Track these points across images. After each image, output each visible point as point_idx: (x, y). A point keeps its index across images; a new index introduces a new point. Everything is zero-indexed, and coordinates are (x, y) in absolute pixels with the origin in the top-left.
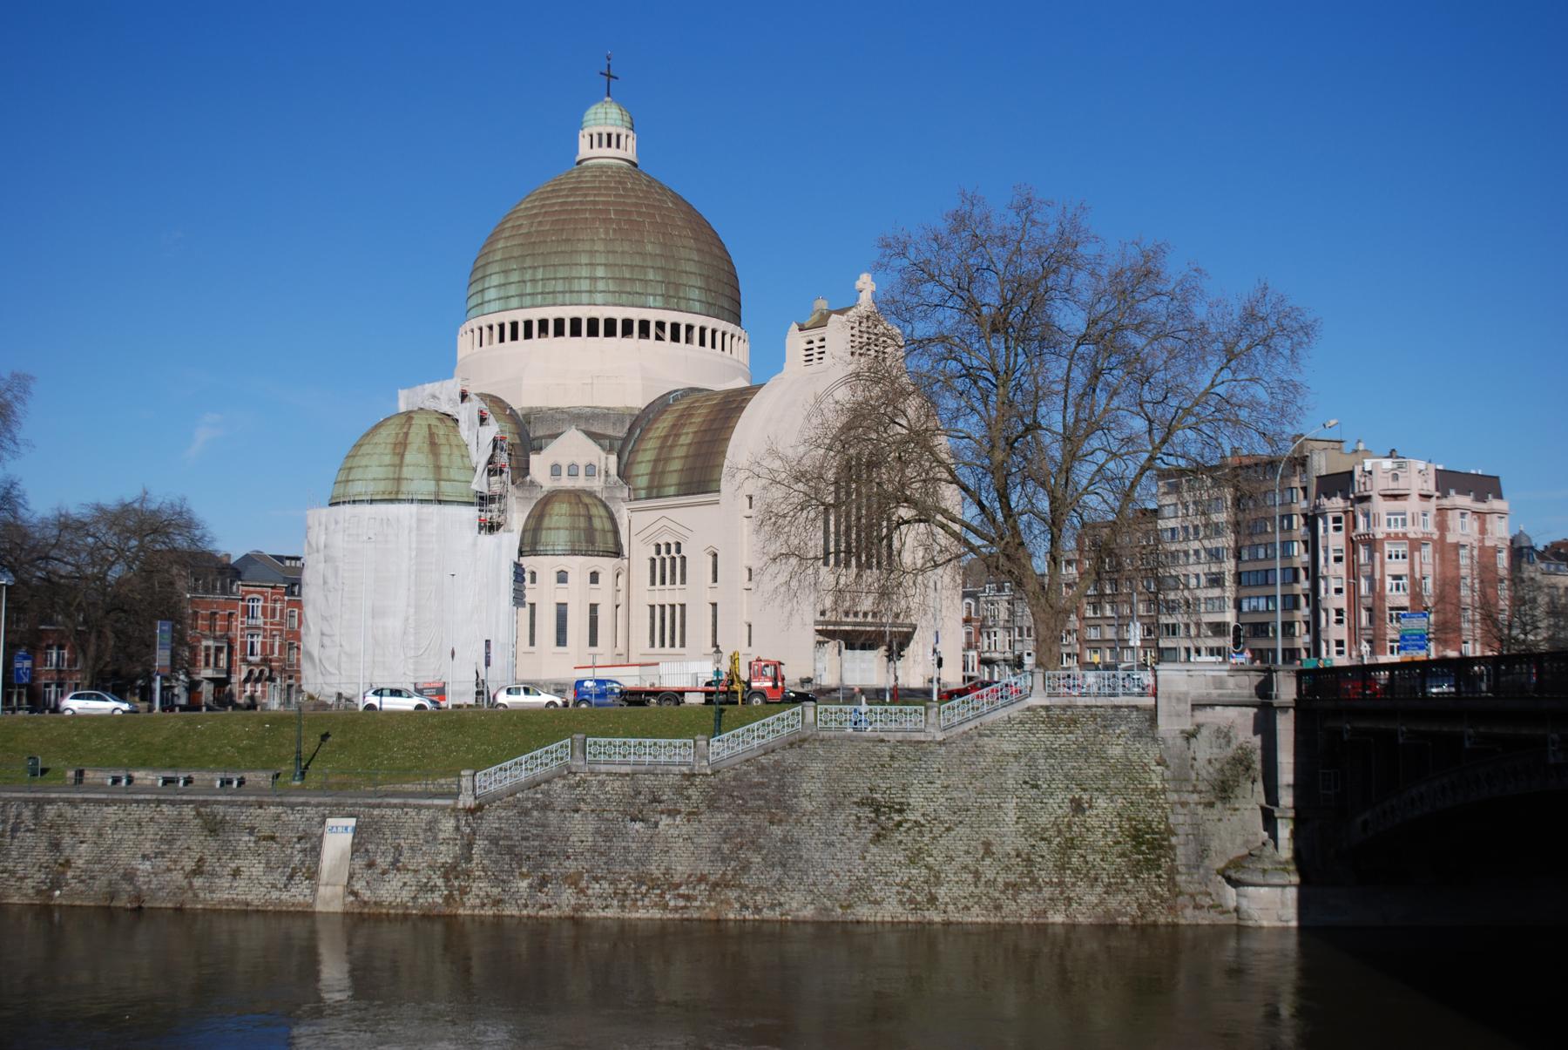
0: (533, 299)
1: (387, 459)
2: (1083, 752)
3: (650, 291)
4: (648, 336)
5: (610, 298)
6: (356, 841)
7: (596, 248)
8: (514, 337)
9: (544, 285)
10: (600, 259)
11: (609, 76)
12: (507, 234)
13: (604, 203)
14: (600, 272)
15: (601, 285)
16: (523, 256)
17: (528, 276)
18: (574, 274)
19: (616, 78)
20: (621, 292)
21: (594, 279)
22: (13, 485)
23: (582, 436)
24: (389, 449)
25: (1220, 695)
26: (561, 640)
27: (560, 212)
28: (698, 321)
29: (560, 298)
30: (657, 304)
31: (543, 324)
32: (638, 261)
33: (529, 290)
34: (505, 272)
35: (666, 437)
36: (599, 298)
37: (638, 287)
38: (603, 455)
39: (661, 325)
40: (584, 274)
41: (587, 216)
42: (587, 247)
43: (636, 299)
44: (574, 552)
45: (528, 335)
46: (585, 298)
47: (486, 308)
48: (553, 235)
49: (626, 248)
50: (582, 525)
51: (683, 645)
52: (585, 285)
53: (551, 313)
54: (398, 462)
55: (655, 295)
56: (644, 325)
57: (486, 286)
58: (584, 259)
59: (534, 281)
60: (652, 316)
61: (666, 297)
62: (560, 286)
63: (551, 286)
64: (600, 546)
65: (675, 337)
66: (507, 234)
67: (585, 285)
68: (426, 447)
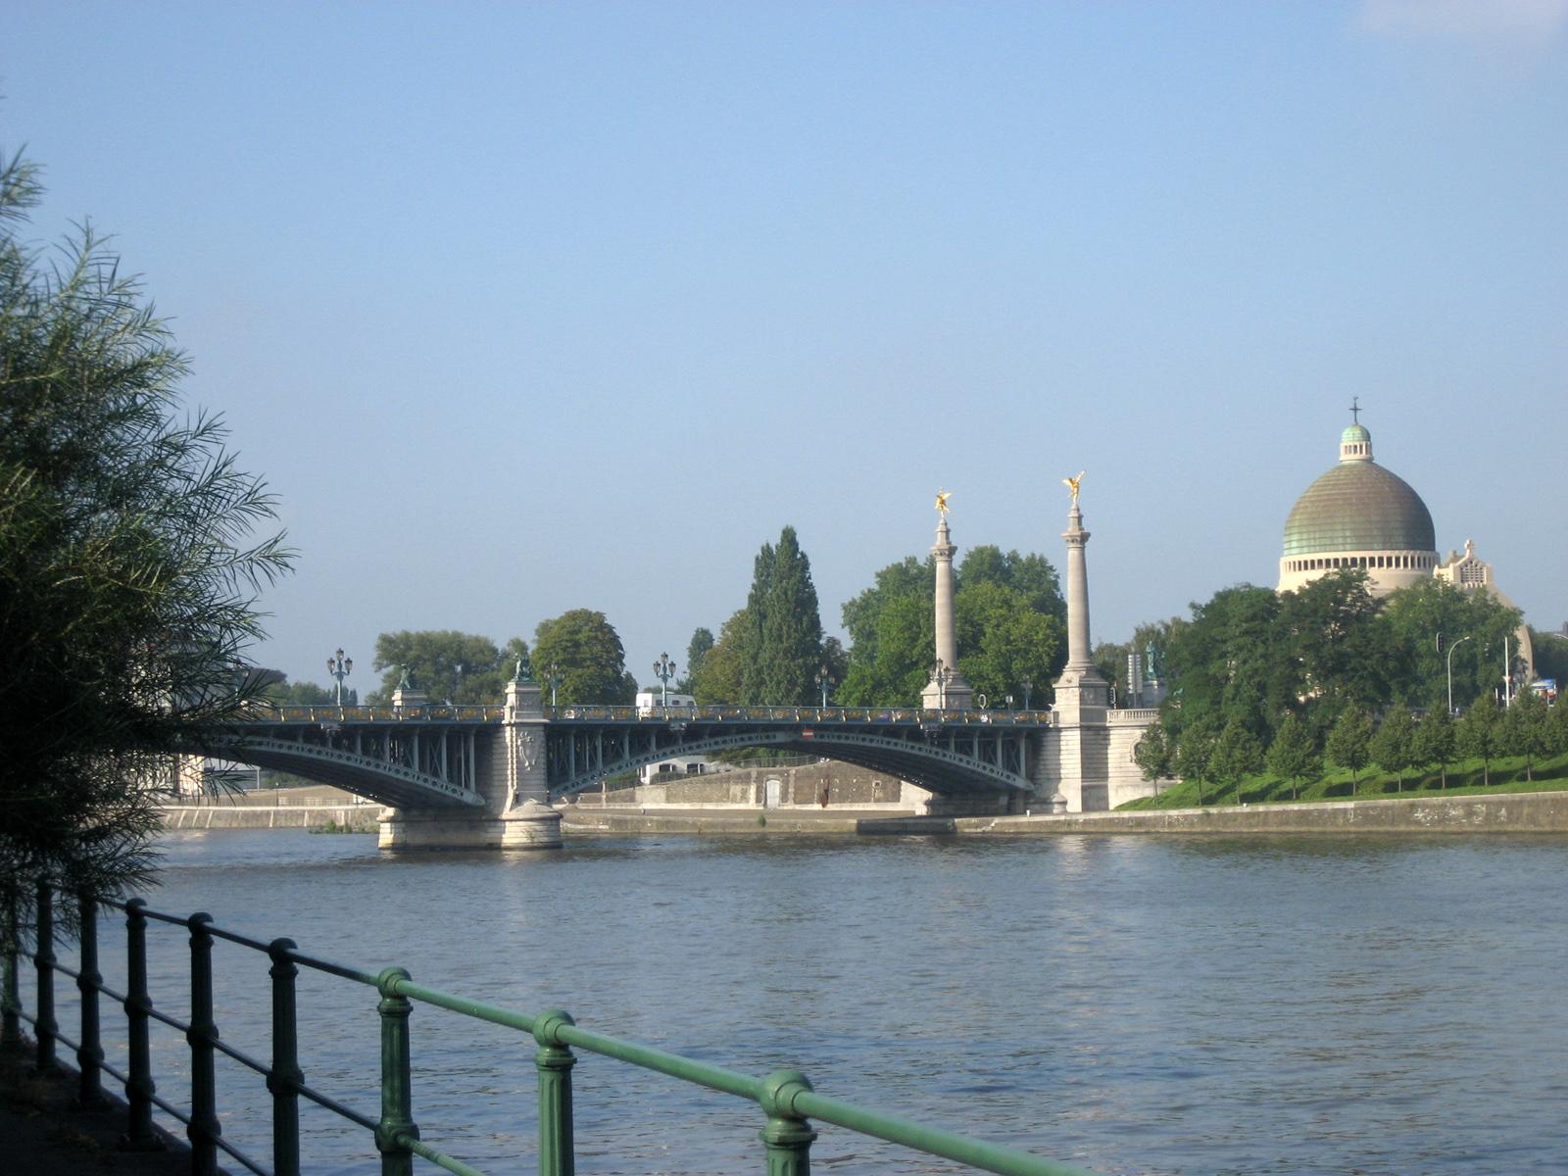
0: (1324, 548)
2: (134, 328)
6: (922, 641)
8: (1300, 569)
12: (1301, 511)
14: (1348, 534)
15: (1349, 540)
16: (1309, 525)
17: (1312, 536)
18: (1335, 535)
19: (194, 374)
20: (1310, 539)
21: (1345, 537)
22: (376, 671)
27: (1328, 500)
31: (1320, 562)
33: (1313, 544)
34: (1300, 533)
36: (1348, 547)
46: (1341, 547)
52: (1340, 540)
56: (1381, 559)
58: (1339, 527)
59: (1314, 539)
63: (1324, 541)
65: (1381, 565)
66: (1301, 511)
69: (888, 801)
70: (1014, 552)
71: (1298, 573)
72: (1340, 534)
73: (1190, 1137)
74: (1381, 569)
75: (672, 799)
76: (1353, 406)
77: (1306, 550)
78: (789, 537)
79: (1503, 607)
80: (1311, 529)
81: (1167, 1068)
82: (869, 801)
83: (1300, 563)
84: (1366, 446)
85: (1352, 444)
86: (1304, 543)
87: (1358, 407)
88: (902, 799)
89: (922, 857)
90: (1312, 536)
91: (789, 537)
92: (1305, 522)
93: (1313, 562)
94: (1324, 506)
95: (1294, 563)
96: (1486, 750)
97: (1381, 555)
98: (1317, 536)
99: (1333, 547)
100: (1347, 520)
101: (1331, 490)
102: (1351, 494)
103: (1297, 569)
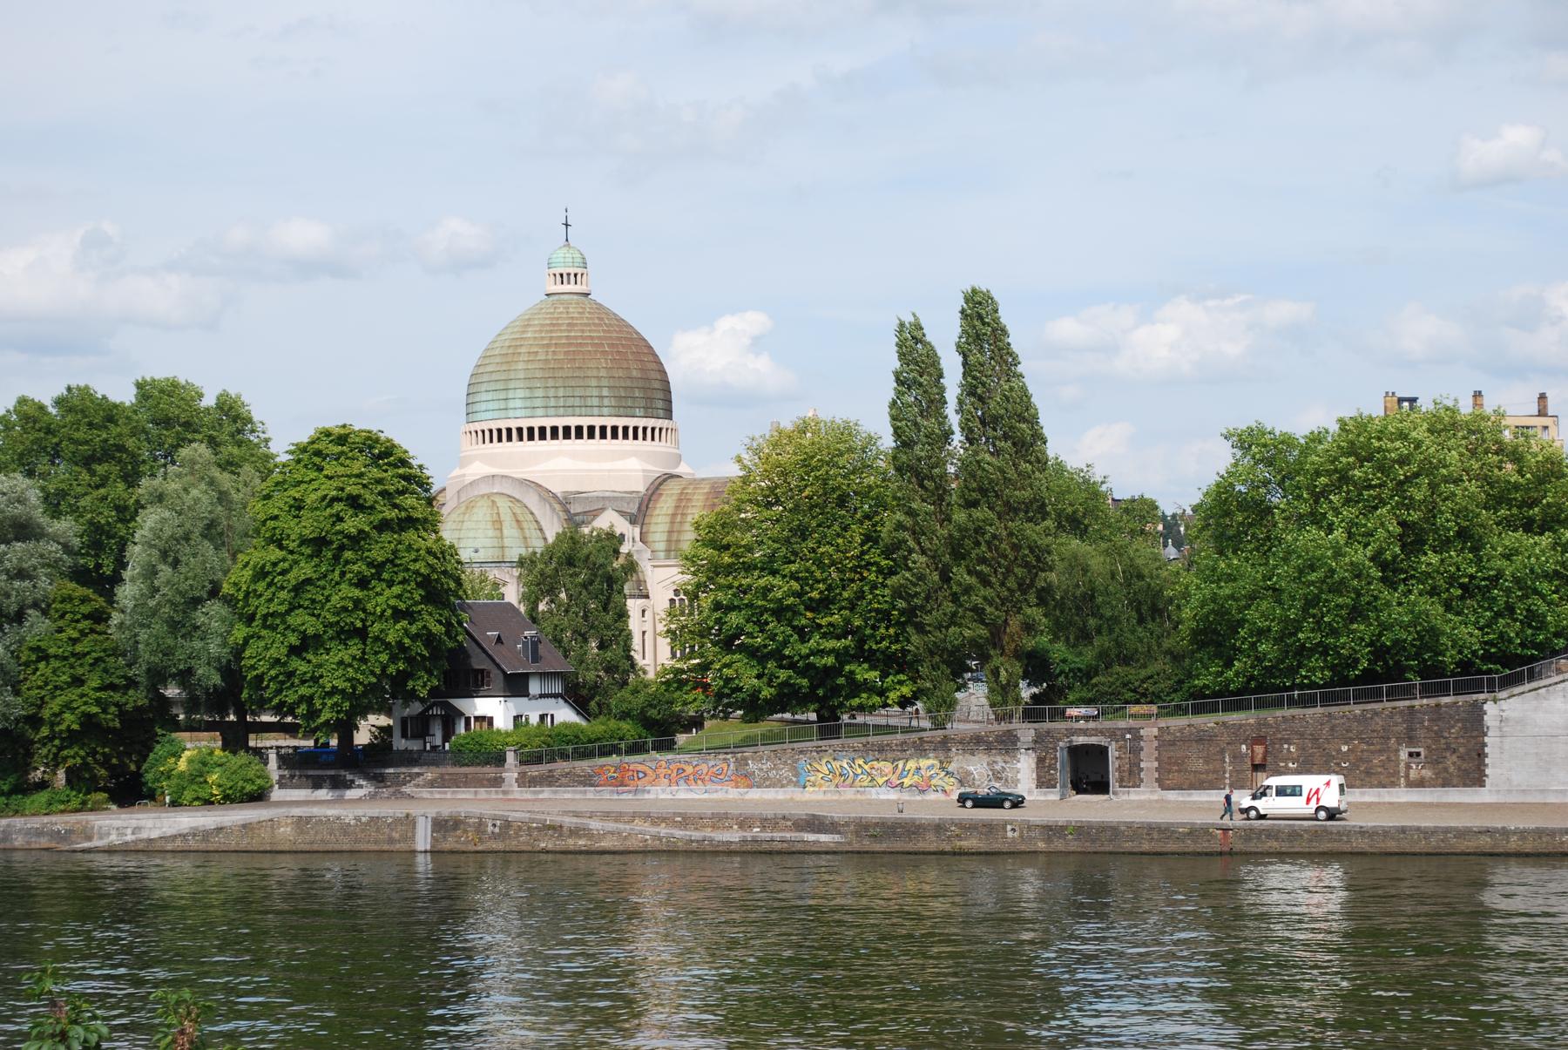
0: (570, 410)
1: (491, 533)
4: (545, 439)
5: (613, 411)
7: (601, 375)
8: (521, 439)
9: (565, 401)
10: (605, 383)
13: (599, 338)
14: (605, 392)
15: (606, 402)
20: (619, 407)
21: (601, 397)
24: (489, 526)
25: (744, 841)
28: (641, 423)
29: (577, 411)
30: (642, 414)
32: (629, 383)
35: (674, 515)
36: (605, 411)
38: (630, 527)
39: (520, 430)
40: (594, 394)
41: (590, 349)
42: (595, 373)
43: (629, 411)
45: (510, 439)
46: (596, 411)
47: (511, 413)
48: (568, 363)
49: (621, 375)
52: (595, 402)
54: (499, 535)
57: (510, 396)
58: (594, 383)
62: (577, 402)
63: (570, 402)
68: (514, 523)
69: (1446, 784)
70: (22, 401)
72: (595, 392)
73: (116, 869)
75: (1175, 777)
79: (1371, 418)
80: (551, 383)
82: (1393, 785)
83: (509, 430)
88: (1488, 781)
89: (201, 829)
90: (551, 393)
92: (539, 374)
96: (278, 709)
98: (561, 393)
99: (586, 409)
100: (603, 373)
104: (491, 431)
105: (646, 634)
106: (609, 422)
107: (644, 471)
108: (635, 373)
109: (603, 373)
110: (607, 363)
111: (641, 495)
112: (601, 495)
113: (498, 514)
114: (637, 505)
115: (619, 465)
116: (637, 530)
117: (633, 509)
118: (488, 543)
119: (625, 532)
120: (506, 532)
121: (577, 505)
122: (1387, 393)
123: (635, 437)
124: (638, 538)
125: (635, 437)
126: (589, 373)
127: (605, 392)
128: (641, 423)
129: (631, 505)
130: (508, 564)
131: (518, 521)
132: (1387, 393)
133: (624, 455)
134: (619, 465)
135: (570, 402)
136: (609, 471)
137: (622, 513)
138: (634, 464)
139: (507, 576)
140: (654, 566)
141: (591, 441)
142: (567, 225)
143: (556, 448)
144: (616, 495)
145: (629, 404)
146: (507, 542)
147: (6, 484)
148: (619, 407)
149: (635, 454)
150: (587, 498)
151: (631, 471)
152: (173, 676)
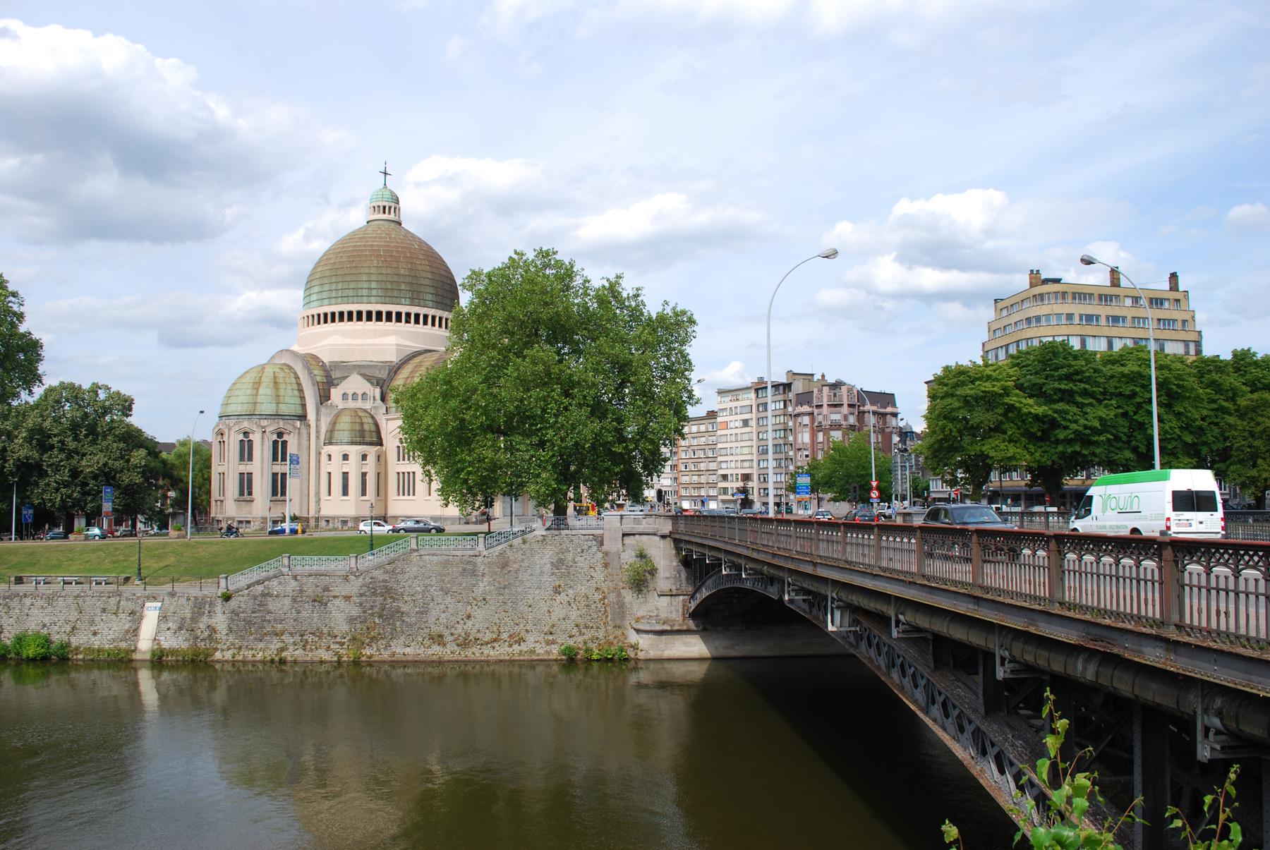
0: (346, 299)
3: (402, 296)
5: (379, 299)
8: (326, 322)
10: (374, 278)
11: (385, 174)
14: (374, 285)
15: (374, 293)
20: (385, 297)
23: (359, 378)
26: (345, 492)
28: (431, 312)
30: (407, 303)
32: (396, 279)
35: (408, 378)
36: (373, 299)
37: (395, 293)
38: (372, 388)
40: (365, 286)
42: (367, 270)
44: (352, 443)
45: (425, 323)
46: (365, 299)
49: (389, 272)
50: (357, 429)
51: (414, 495)
52: (365, 292)
53: (355, 308)
55: (405, 298)
58: (365, 278)
60: (404, 309)
61: (412, 299)
63: (346, 293)
64: (368, 439)
67: (365, 292)
68: (271, 385)
71: (323, 325)
74: (425, 327)
76: (383, 170)
77: (326, 302)
78: (926, 383)
80: (334, 279)
81: (301, 390)
83: (326, 315)
84: (395, 208)
85: (380, 204)
86: (325, 295)
87: (388, 172)
91: (926, 383)
93: (333, 314)
94: (349, 257)
95: (319, 315)
97: (408, 311)
99: (357, 298)
100: (373, 270)
101: (358, 242)
102: (379, 246)
103: (411, 493)
104: (319, 315)
105: (368, 477)
106: (374, 308)
107: (397, 345)
108: (402, 272)
109: (373, 270)
110: (378, 263)
111: (393, 364)
112: (358, 363)
113: (261, 377)
114: (387, 372)
115: (378, 341)
116: (378, 391)
117: (383, 375)
118: (245, 399)
119: (368, 392)
120: (261, 391)
121: (337, 371)
122: (1032, 271)
123: (433, 324)
124: (378, 397)
125: (433, 324)
126: (363, 271)
127: (374, 285)
128: (431, 312)
129: (382, 372)
130: (258, 417)
131: (276, 383)
132: (1032, 271)
133: (385, 333)
134: (378, 341)
135: (346, 293)
136: (369, 345)
137: (368, 378)
138: (392, 340)
139: (255, 426)
140: (388, 420)
141: (350, 323)
142: (385, 174)
143: (352, 328)
144: (371, 363)
145: (395, 295)
146: (260, 399)
147: (1130, 365)
148: (385, 297)
149: (395, 333)
150: (346, 366)
151: (386, 345)
152: (119, 487)
